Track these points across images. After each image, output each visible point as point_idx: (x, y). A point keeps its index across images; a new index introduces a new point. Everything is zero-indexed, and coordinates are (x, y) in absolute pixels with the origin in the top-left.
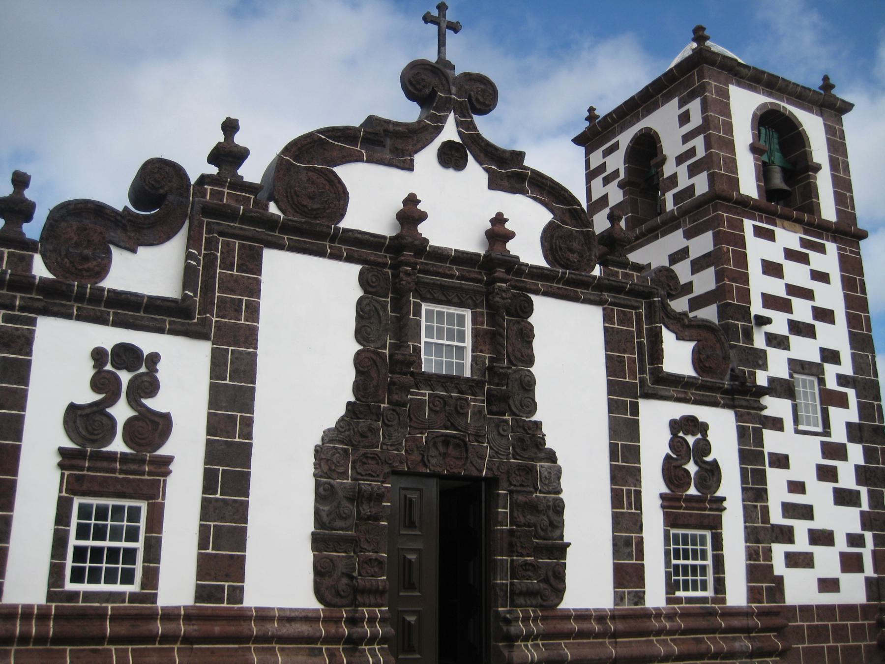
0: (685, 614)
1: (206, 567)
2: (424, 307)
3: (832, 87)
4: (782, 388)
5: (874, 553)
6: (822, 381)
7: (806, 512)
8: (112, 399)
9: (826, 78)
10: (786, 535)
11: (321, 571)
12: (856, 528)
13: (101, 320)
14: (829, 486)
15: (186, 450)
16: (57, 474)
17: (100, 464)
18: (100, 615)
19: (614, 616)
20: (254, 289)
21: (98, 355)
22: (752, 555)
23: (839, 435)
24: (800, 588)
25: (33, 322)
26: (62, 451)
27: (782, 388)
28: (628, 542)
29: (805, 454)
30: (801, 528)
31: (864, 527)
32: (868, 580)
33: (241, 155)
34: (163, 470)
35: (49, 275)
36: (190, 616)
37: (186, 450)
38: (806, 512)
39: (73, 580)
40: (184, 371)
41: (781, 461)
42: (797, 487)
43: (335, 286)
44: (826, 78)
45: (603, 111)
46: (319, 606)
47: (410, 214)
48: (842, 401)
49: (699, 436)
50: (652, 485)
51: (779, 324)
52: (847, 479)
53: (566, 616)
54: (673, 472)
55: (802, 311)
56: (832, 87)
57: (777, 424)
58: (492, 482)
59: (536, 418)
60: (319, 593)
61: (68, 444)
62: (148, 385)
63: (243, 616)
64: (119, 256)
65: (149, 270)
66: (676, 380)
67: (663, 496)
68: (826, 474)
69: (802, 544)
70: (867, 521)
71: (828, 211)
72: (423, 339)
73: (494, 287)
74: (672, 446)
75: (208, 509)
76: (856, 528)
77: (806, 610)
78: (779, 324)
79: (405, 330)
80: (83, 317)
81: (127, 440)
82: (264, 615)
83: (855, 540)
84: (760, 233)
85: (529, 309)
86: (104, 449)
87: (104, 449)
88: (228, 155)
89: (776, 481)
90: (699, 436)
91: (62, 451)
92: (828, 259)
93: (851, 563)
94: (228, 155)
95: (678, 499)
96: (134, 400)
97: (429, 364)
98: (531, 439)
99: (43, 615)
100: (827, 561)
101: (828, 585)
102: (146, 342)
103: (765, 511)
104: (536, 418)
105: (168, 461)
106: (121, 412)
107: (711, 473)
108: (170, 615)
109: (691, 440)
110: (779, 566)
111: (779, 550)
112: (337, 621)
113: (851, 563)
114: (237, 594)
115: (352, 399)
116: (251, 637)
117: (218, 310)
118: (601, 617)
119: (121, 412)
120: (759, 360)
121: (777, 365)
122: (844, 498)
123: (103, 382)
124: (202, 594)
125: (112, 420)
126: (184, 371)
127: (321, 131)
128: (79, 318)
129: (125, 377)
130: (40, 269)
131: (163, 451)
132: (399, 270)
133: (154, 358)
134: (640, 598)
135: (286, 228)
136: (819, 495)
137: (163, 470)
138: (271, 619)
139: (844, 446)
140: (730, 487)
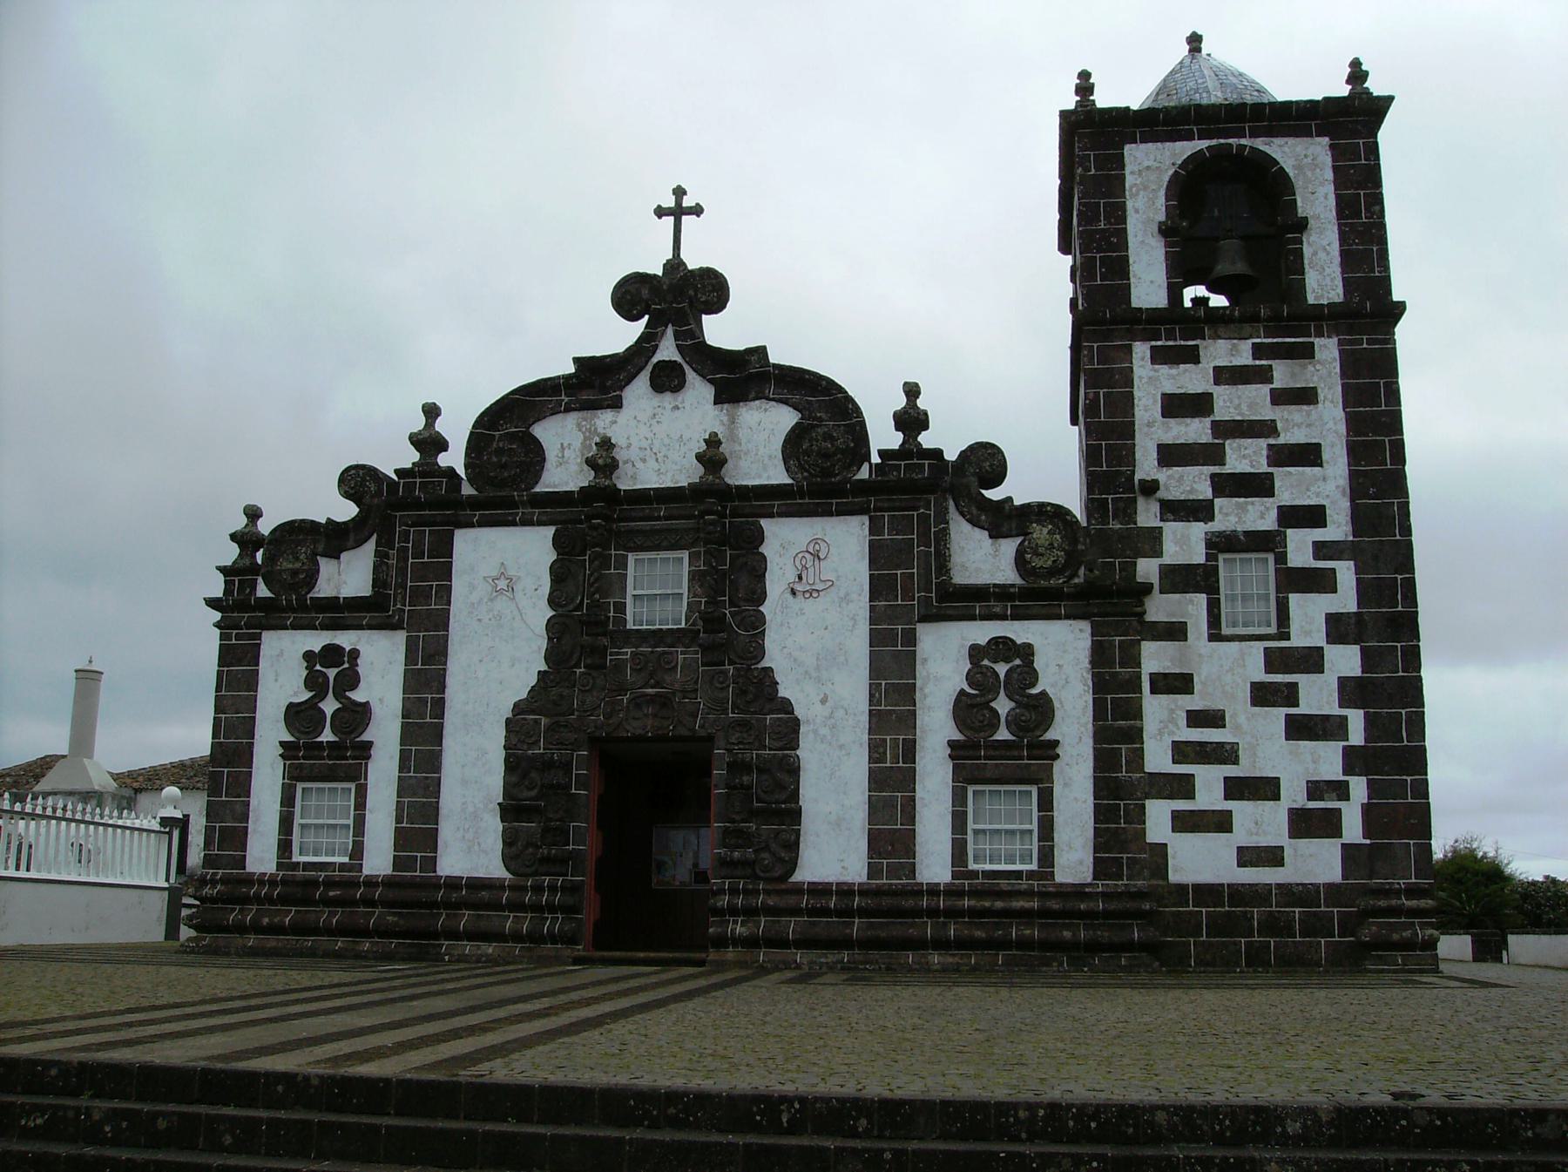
0: (975, 893)
1: (402, 839)
2: (631, 557)
4: (1181, 579)
5: (1367, 810)
6: (1281, 558)
7: (1223, 754)
8: (321, 695)
9: (1356, 64)
10: (1182, 787)
11: (509, 840)
13: (310, 626)
14: (1279, 714)
15: (385, 733)
16: (280, 763)
17: (1035, 752)
18: (314, 883)
19: (864, 891)
20: (446, 572)
21: (309, 656)
22: (1102, 814)
24: (1198, 861)
25: (259, 637)
26: (952, 744)
27: (1181, 579)
28: (890, 804)
29: (1227, 670)
31: (1348, 770)
32: (1346, 847)
33: (441, 445)
34: (1050, 752)
35: (269, 594)
36: (388, 882)
37: (385, 733)
38: (1223, 754)
39: (976, 861)
40: (381, 662)
43: (527, 552)
46: (507, 875)
47: (604, 459)
48: (1320, 582)
51: (1193, 482)
53: (798, 890)
55: (1244, 457)
58: (710, 739)
59: (765, 663)
60: (508, 860)
61: (288, 738)
62: (351, 679)
63: (436, 884)
64: (326, 566)
65: (349, 576)
66: (979, 594)
67: (952, 744)
70: (1354, 760)
71: (1323, 280)
72: (630, 591)
73: (717, 522)
74: (969, 677)
75: (403, 788)
77: (1207, 893)
78: (1193, 482)
79: (609, 585)
80: (296, 626)
81: (334, 730)
82: (453, 883)
84: (1159, 357)
85: (759, 537)
88: (429, 443)
91: (952, 744)
92: (1327, 360)
94: (429, 443)
95: (976, 746)
96: (339, 696)
97: (636, 617)
98: (760, 690)
99: (272, 881)
102: (345, 639)
104: (765, 663)
105: (369, 745)
106: (329, 706)
108: (371, 882)
109: (1002, 669)
112: (524, 889)
113: (1306, 824)
114: (432, 863)
115: (544, 667)
116: (922, 910)
117: (414, 603)
118: (845, 890)
119: (329, 706)
120: (1152, 542)
121: (1185, 543)
122: (1302, 728)
123: (314, 682)
124: (398, 863)
125: (995, 713)
126: (381, 662)
127: (512, 393)
128: (295, 627)
129: (332, 673)
130: (263, 591)
131: (365, 737)
132: (600, 524)
133: (355, 654)
135: (473, 503)
137: (1050, 752)
138: (376, 884)
139: (1319, 651)
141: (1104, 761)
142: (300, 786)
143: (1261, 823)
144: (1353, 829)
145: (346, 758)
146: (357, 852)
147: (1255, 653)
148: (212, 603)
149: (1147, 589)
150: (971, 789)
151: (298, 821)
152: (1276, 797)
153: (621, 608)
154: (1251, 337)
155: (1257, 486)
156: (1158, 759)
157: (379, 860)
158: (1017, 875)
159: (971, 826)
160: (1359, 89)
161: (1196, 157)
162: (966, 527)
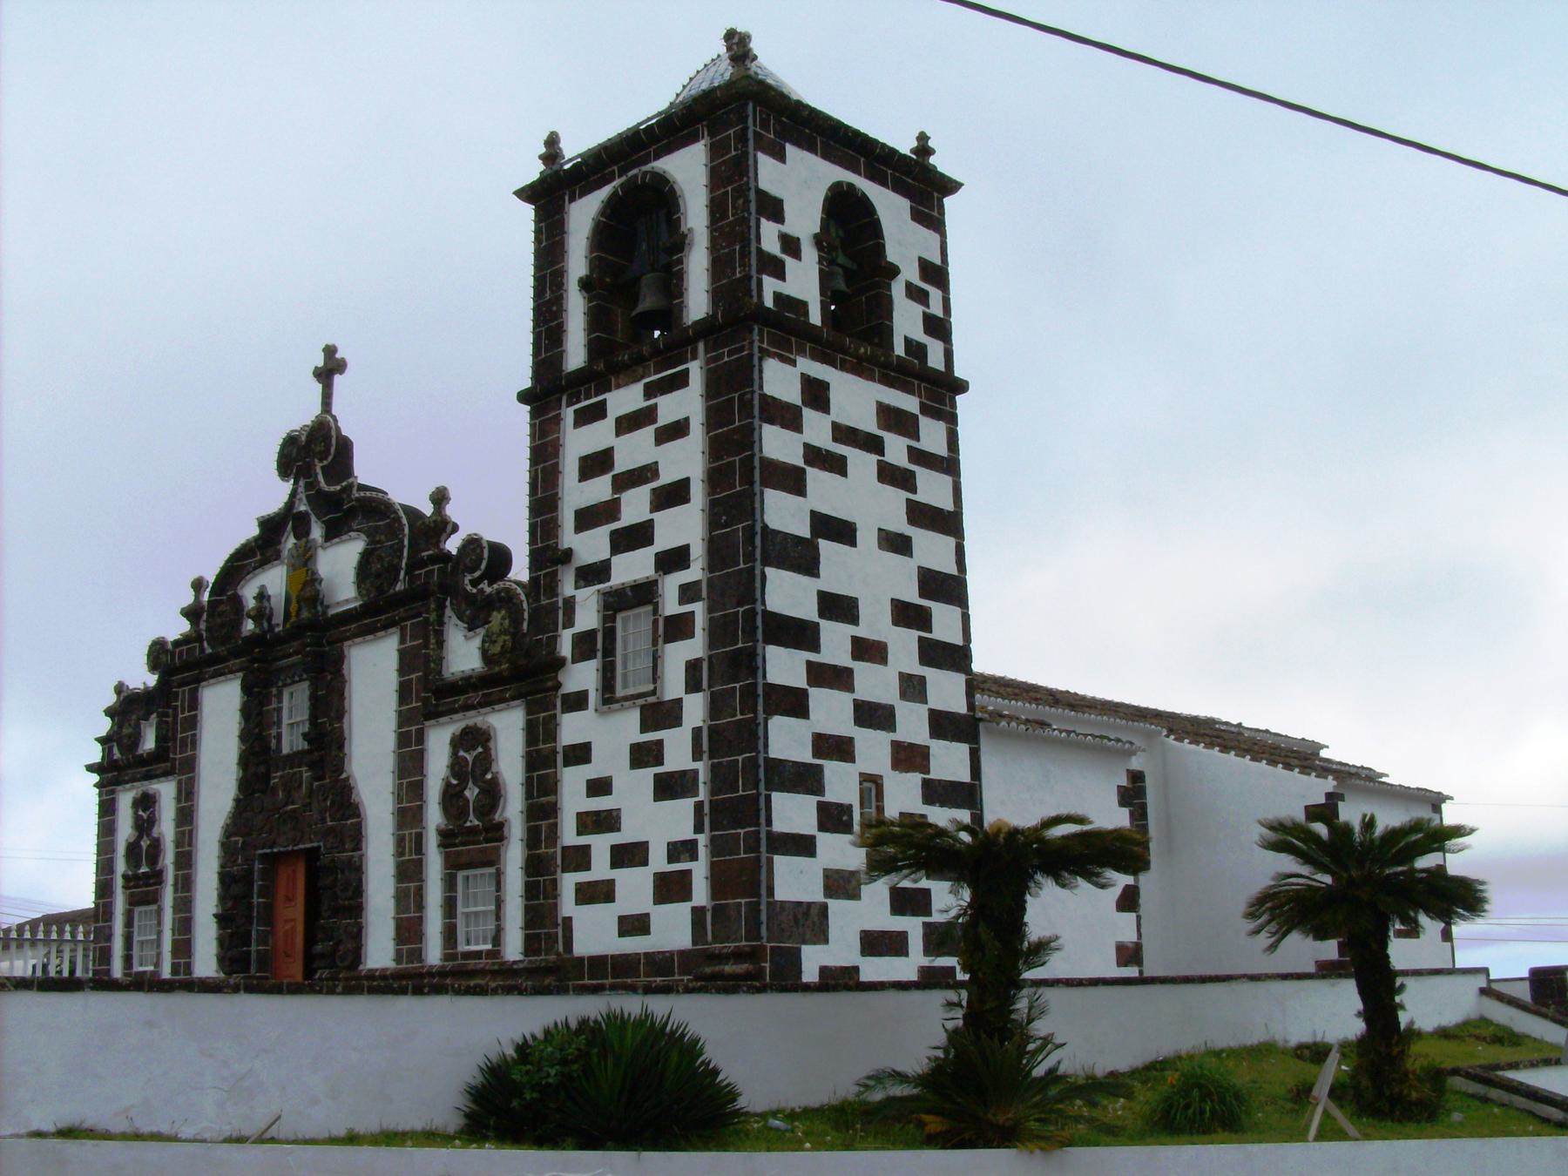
3: (930, 152)
5: (714, 867)
10: (579, 858)
12: (685, 831)
23: (673, 685)
30: (601, 845)
41: (580, 754)
42: (599, 787)
44: (923, 138)
45: (573, 148)
48: (678, 628)
49: (480, 750)
50: (434, 816)
52: (678, 752)
54: (451, 797)
55: (635, 506)
56: (930, 152)
57: (577, 702)
68: (644, 755)
69: (600, 868)
72: (285, 721)
76: (683, 829)
83: (680, 850)
86: (604, 193)
87: (604, 193)
89: (572, 784)
90: (480, 750)
93: (671, 888)
100: (635, 889)
101: (634, 925)
103: (554, 829)
107: (492, 793)
110: (567, 905)
111: (569, 882)
113: (671, 888)
122: (669, 787)
134: (418, 954)
136: (632, 790)
140: (513, 808)
141: (532, 839)
142: (461, 875)
143: (635, 889)
144: (701, 893)
145: (479, 843)
146: (497, 939)
147: (633, 718)
148: (91, 768)
149: (561, 663)
150: (461, 875)
151: (136, 938)
152: (645, 863)
153: (279, 737)
154: (643, 377)
155: (637, 536)
156: (569, 835)
157: (66, 974)
158: (478, 954)
159: (460, 909)
160: (556, 167)
161: (614, 195)
162: (455, 619)
